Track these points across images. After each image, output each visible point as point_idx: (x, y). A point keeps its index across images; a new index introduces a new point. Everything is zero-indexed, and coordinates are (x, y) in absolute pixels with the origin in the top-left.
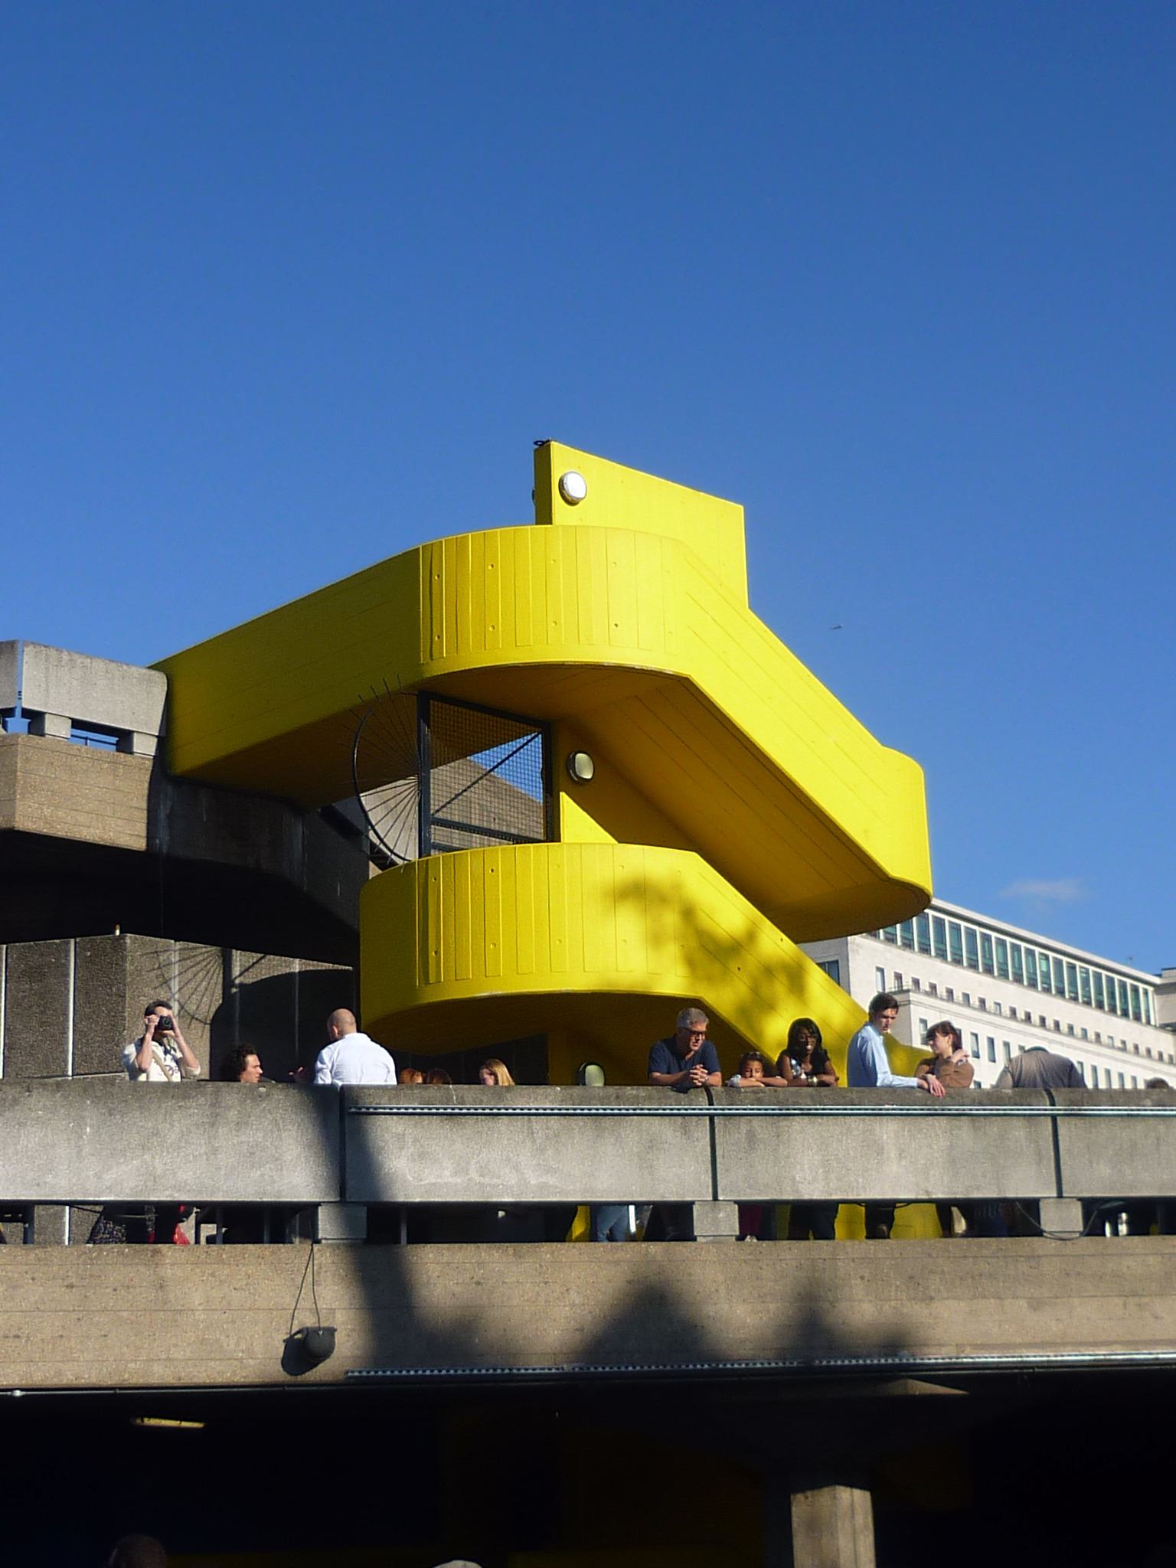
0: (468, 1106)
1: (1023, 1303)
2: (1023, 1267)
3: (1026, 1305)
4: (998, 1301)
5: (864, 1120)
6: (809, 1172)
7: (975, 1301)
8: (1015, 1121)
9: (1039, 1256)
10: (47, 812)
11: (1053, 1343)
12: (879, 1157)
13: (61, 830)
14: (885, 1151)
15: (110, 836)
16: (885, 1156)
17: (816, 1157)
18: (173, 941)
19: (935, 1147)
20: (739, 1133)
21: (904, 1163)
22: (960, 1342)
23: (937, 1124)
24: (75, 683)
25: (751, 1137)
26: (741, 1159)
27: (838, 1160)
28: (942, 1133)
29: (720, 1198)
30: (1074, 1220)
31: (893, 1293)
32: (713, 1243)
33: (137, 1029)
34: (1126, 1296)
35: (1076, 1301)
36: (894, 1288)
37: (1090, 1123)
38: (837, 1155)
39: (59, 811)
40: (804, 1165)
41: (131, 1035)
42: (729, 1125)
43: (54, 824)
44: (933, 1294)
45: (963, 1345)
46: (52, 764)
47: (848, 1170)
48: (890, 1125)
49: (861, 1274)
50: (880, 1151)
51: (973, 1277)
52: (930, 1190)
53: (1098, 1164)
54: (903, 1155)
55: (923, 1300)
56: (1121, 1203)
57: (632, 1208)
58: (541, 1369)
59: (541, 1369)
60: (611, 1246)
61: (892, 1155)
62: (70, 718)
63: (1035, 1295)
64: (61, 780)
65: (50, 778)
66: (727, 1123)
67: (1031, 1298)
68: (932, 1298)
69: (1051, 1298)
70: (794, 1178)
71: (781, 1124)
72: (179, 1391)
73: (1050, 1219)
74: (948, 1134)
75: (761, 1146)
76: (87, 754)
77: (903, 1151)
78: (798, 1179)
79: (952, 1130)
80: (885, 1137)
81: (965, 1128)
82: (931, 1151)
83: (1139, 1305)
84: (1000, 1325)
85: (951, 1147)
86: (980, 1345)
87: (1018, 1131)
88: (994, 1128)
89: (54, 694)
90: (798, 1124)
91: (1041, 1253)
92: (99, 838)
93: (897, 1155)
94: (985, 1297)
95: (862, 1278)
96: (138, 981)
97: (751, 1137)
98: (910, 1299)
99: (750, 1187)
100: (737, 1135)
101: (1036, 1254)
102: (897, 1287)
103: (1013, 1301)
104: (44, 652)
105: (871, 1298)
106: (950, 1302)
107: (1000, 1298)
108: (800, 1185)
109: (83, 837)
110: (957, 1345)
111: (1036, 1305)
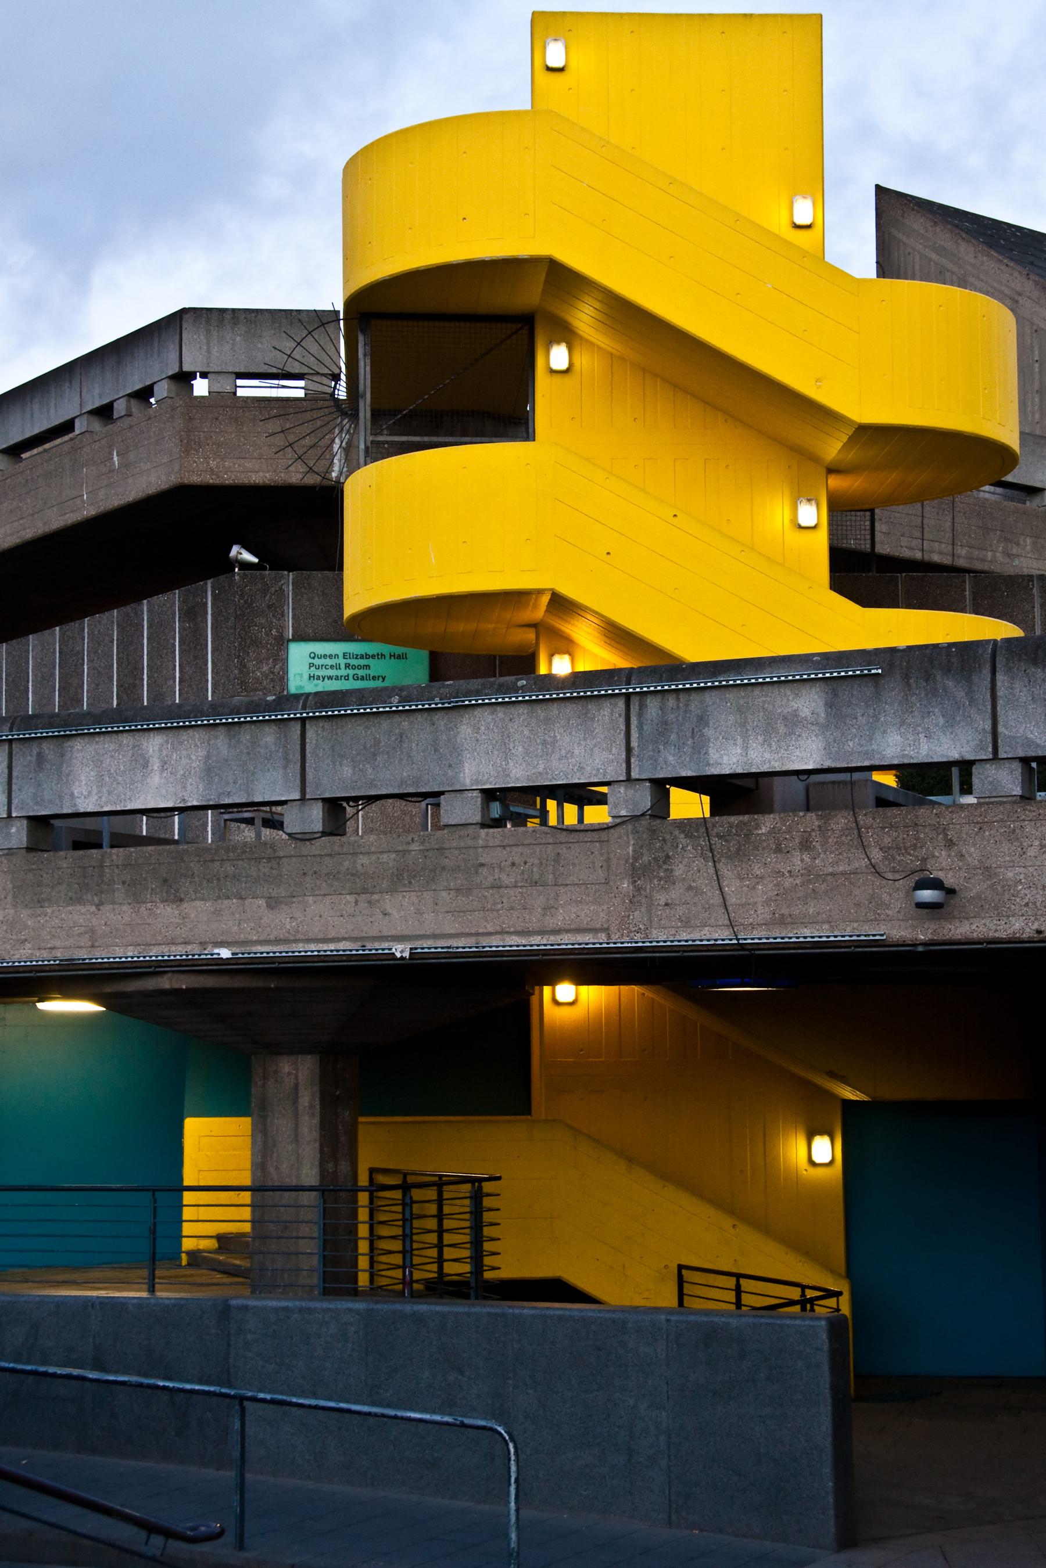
0: (41, 731)
1: (262, 902)
2: (264, 868)
3: (265, 905)
4: (240, 901)
5: (134, 736)
6: (85, 788)
7: (220, 901)
8: (267, 728)
9: (280, 858)
10: (213, 464)
11: (285, 940)
12: (144, 771)
13: (228, 478)
14: (150, 765)
15: (281, 477)
16: (150, 768)
17: (92, 773)
18: (286, 572)
19: (194, 758)
20: (31, 755)
21: (165, 775)
22: (203, 941)
23: (197, 736)
24: (238, 339)
25: (40, 759)
26: (31, 779)
27: (110, 774)
28: (201, 744)
29: (14, 815)
30: (315, 817)
31: (148, 896)
32: (8, 854)
33: (248, 656)
34: (358, 894)
35: (310, 899)
36: (149, 890)
37: (337, 724)
38: (110, 770)
39: (226, 461)
40: (82, 781)
41: (241, 662)
42: (24, 749)
43: (221, 474)
44: (183, 896)
45: (206, 943)
46: (217, 419)
47: (118, 783)
48: (156, 739)
49: (123, 880)
50: (146, 765)
51: (219, 880)
52: (186, 798)
53: (341, 765)
54: (165, 767)
55: (173, 902)
56: (408, 799)
57: (955, 771)
58: (865, 936)
59: (865, 936)
60: (487, 835)
61: (156, 768)
62: (232, 373)
63: (273, 895)
64: (227, 432)
65: (216, 432)
66: (22, 747)
67: (269, 898)
68: (181, 900)
69: (288, 897)
70: (72, 795)
71: (65, 744)
72: (691, 954)
73: (294, 820)
74: (206, 744)
75: (48, 766)
76: (253, 404)
77: (165, 763)
78: (76, 794)
79: (210, 740)
80: (151, 751)
81: (221, 737)
82: (189, 762)
83: (370, 902)
84: (239, 923)
85: (208, 757)
86: (221, 942)
87: (269, 737)
88: (246, 736)
89: (216, 353)
90: (78, 744)
91: (281, 854)
92: (269, 480)
93: (160, 768)
94: (228, 898)
95: (124, 883)
96: (248, 613)
97: (40, 759)
98: (162, 902)
99: (37, 803)
100: (29, 758)
101: (277, 854)
102: (152, 890)
103: (253, 900)
104: (205, 315)
105: (129, 901)
106: (198, 903)
107: (241, 898)
108: (78, 800)
109: (252, 481)
110: (201, 943)
111: (273, 903)
